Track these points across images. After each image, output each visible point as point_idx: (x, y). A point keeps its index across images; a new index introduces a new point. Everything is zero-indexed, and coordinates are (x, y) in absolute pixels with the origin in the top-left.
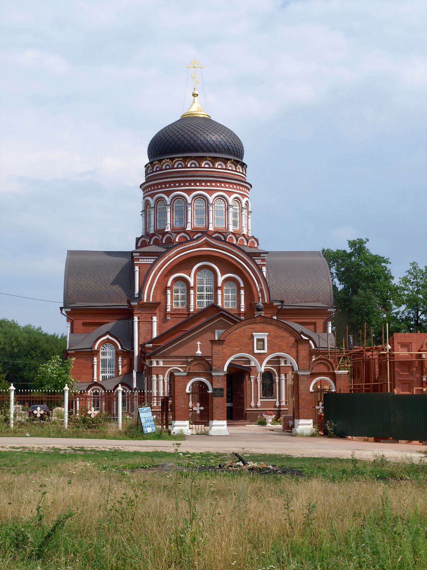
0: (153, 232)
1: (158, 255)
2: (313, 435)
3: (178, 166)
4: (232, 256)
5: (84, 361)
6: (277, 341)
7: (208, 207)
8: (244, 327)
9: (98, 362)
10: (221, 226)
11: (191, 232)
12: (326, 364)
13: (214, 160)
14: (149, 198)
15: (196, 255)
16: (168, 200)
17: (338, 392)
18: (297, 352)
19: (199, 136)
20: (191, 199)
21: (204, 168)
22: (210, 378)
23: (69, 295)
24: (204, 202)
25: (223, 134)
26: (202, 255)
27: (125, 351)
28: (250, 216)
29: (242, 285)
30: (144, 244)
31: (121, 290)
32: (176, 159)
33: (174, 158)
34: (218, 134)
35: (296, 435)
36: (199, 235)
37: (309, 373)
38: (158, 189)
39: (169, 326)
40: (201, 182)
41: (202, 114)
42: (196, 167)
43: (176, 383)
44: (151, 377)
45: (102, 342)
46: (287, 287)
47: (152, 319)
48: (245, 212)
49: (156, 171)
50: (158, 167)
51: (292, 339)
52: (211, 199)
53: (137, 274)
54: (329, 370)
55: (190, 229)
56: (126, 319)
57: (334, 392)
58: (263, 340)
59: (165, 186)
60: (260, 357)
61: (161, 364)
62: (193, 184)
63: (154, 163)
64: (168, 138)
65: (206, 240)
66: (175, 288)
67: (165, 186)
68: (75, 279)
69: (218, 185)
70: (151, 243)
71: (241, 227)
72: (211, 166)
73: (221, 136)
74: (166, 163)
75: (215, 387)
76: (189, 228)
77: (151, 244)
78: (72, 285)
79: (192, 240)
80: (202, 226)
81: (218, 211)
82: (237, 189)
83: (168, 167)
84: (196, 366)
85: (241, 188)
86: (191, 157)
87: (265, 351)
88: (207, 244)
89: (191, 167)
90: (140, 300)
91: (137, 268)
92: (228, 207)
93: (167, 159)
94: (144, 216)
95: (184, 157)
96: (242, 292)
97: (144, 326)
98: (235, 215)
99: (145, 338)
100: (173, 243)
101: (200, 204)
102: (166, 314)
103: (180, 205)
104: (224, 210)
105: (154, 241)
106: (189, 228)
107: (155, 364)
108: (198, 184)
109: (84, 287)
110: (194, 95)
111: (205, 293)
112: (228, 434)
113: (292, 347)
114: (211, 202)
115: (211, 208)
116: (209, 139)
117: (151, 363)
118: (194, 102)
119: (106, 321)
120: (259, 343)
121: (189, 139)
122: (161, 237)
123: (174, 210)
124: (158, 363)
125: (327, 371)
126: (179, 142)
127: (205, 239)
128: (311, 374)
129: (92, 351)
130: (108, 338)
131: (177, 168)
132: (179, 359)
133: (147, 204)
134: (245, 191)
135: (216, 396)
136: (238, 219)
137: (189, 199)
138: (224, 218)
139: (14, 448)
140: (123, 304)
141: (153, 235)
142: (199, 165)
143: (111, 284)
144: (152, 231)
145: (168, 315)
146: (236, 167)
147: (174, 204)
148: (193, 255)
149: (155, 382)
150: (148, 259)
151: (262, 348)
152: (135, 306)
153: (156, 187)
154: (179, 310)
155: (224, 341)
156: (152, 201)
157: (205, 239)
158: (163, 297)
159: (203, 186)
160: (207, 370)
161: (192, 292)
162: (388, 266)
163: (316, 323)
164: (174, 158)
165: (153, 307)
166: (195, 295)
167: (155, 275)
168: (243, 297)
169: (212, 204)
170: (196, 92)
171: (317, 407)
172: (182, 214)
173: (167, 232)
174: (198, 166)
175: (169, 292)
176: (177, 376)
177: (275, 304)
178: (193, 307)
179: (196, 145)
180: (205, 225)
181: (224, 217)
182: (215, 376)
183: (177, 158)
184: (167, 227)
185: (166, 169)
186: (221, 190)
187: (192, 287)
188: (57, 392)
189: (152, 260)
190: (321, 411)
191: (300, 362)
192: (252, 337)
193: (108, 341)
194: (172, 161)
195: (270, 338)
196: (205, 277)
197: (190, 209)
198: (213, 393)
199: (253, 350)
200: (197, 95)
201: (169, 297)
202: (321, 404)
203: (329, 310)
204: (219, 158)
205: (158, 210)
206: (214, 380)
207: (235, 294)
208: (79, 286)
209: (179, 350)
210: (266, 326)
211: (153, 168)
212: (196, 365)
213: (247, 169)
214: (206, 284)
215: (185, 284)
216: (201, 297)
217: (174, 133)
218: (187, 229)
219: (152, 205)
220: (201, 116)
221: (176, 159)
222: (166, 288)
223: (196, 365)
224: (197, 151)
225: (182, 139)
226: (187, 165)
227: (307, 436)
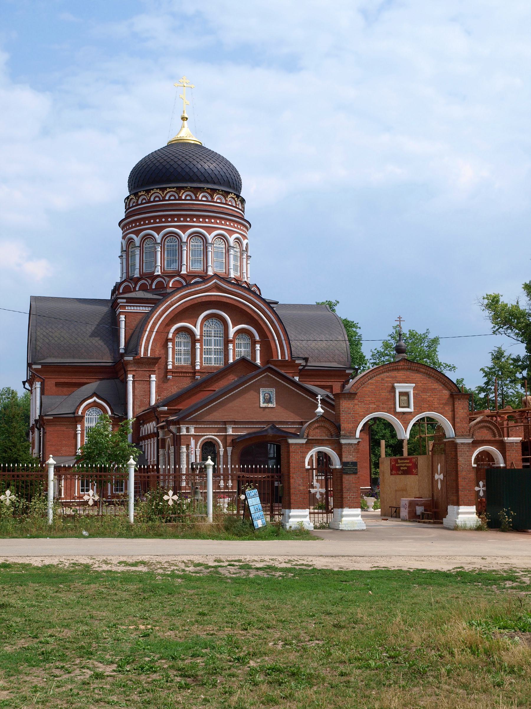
0: (138, 276)
1: (156, 303)
2: (479, 529)
3: (169, 196)
4: (239, 304)
5: (64, 428)
6: (425, 396)
7: (206, 247)
8: (382, 375)
9: (82, 430)
11: (188, 276)
12: (490, 428)
13: (196, 190)
16: (158, 237)
17: (508, 468)
18: (453, 411)
19: (195, 163)
20: (186, 237)
21: (201, 201)
22: (339, 448)
23: (38, 348)
26: (210, 301)
27: (116, 416)
29: (257, 338)
30: (127, 290)
31: (102, 344)
35: (456, 528)
36: (197, 279)
37: (470, 441)
38: (145, 224)
39: (174, 388)
40: (204, 217)
42: (160, 201)
43: (291, 454)
44: (180, 449)
45: (87, 405)
47: (150, 377)
49: (142, 204)
50: (144, 199)
51: (446, 393)
52: (210, 238)
54: (495, 436)
55: (186, 273)
57: (503, 467)
58: (407, 394)
60: (404, 417)
61: (192, 432)
62: (176, 219)
68: (44, 329)
69: (218, 221)
70: (137, 289)
72: (210, 199)
74: (155, 194)
75: (345, 460)
76: (184, 272)
77: (137, 289)
78: (42, 336)
79: (189, 285)
81: (208, 253)
82: (238, 228)
83: (157, 199)
84: (316, 430)
85: (242, 228)
87: (411, 409)
90: (136, 354)
91: (122, 317)
92: (228, 248)
93: (157, 189)
95: (177, 188)
96: (258, 347)
97: (140, 386)
98: (235, 256)
99: (141, 401)
100: (166, 288)
101: (198, 243)
102: (167, 371)
103: (173, 244)
104: (224, 252)
105: (140, 286)
106: (184, 272)
107: (184, 432)
109: (56, 339)
110: (184, 119)
111: (213, 347)
112: (365, 528)
113: (446, 404)
114: (210, 241)
115: (210, 249)
116: (206, 167)
117: (179, 430)
119: (85, 381)
120: (403, 398)
121: (183, 166)
122: (150, 281)
124: (188, 429)
125: (493, 439)
126: (172, 170)
127: (214, 281)
128: (473, 442)
129: (75, 417)
130: (95, 401)
131: (169, 200)
132: (215, 425)
133: (130, 242)
135: (347, 473)
137: (184, 237)
138: (224, 261)
139: (126, 564)
140: (107, 360)
141: (139, 279)
142: (196, 197)
145: (169, 374)
147: (166, 243)
148: (200, 300)
149: (185, 454)
150: (137, 306)
151: (406, 405)
153: (134, 225)
154: (182, 367)
155: (356, 394)
156: (137, 240)
157: (214, 281)
158: (163, 352)
159: (200, 222)
160: (332, 435)
161: (198, 345)
162: (358, 330)
163: (332, 386)
164: (165, 189)
165: (153, 363)
166: (201, 349)
167: (155, 324)
169: (211, 244)
170: (186, 116)
171: (477, 489)
172: (176, 254)
173: (158, 276)
174: (194, 198)
175: (170, 345)
176: (292, 444)
177: (297, 362)
178: (199, 363)
182: (345, 444)
183: (170, 188)
185: (154, 201)
187: (198, 340)
188: (18, 469)
190: (481, 494)
191: (458, 425)
192: (393, 389)
193: (95, 404)
194: (163, 192)
195: (416, 392)
196: (214, 328)
197: (185, 248)
198: (342, 469)
199: (395, 408)
201: (170, 351)
202: (481, 483)
203: (347, 371)
205: (144, 250)
206: (343, 449)
208: (50, 338)
209: (215, 413)
210: (412, 374)
211: (138, 200)
212: (317, 428)
216: (209, 352)
220: (193, 142)
221: (168, 190)
222: (167, 340)
223: (317, 428)
224: (193, 181)
225: (175, 166)
227: (471, 529)
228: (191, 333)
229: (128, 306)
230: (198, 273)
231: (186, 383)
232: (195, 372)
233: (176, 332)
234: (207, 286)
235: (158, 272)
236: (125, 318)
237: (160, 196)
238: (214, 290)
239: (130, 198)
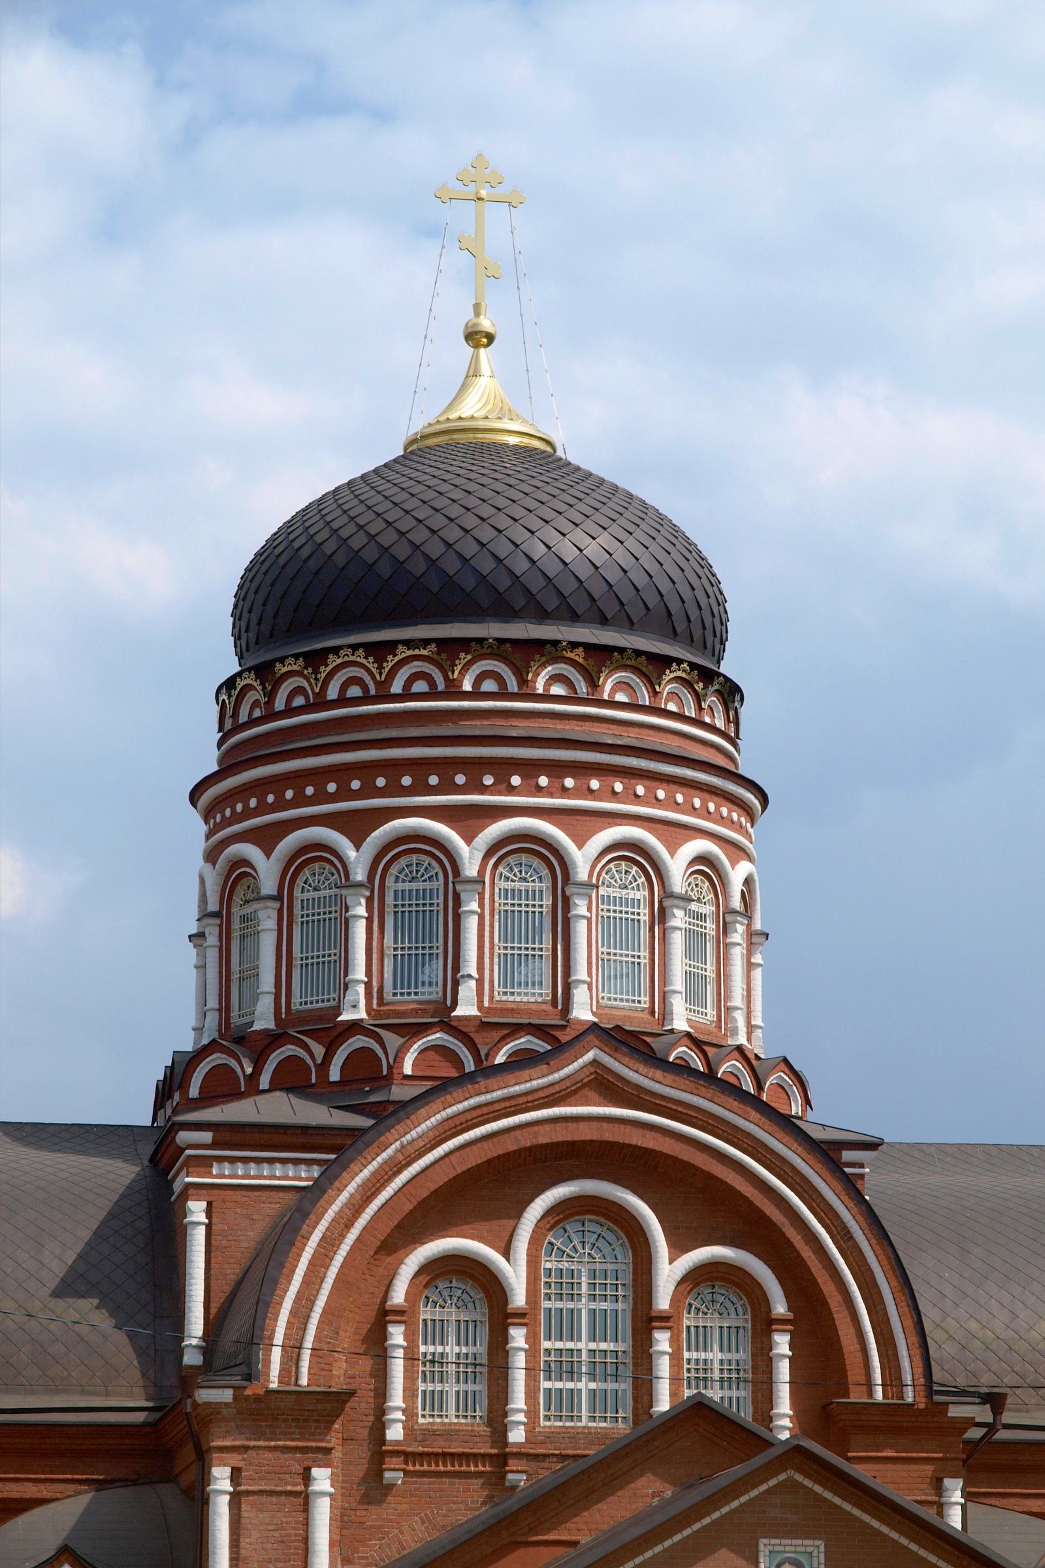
0: (271, 1025)
1: (339, 1147)
7: (567, 901)
10: (629, 1004)
14: (251, 851)
15: (543, 1140)
16: (357, 859)
19: (520, 535)
20: (479, 856)
21: (546, 697)
24: (545, 872)
25: (638, 534)
26: (572, 1144)
28: (757, 959)
29: (780, 1308)
30: (223, 1087)
32: (403, 652)
33: (390, 647)
34: (615, 529)
38: (301, 800)
40: (530, 768)
41: (512, 431)
42: (366, 699)
46: (973, 1326)
47: (307, 1478)
48: (738, 935)
49: (289, 712)
50: (299, 690)
53: (198, 1238)
55: (473, 1011)
56: (135, 1483)
59: (299, 792)
63: (280, 669)
64: (329, 548)
65: (595, 1062)
66: (425, 1313)
67: (299, 792)
70: (265, 1081)
71: (724, 1011)
72: (583, 689)
73: (630, 543)
76: (466, 1008)
79: (487, 1071)
80: (531, 996)
82: (708, 815)
83: (354, 691)
85: (724, 811)
86: (480, 641)
88: (605, 1086)
89: (476, 695)
90: (249, 1378)
91: (197, 1210)
94: (212, 940)
95: (441, 642)
96: (782, 1343)
98: (694, 939)
102: (379, 1451)
103: (420, 885)
104: (645, 918)
105: (276, 1070)
106: (466, 1008)
108: (488, 780)
110: (477, 338)
111: (584, 1345)
115: (580, 907)
116: (570, 554)
118: (473, 372)
122: (319, 1051)
123: (389, 910)
127: (590, 1056)
131: (406, 696)
133: (238, 876)
134: (740, 829)
136: (710, 970)
138: (645, 961)
140: (125, 1399)
141: (273, 1040)
142: (523, 682)
143: (57, 1294)
144: (264, 1021)
146: (699, 699)
147: (390, 882)
148: (526, 1140)
150: (259, 1161)
152: (215, 1409)
154: (449, 1433)
156: (267, 869)
157: (590, 1056)
158: (365, 1364)
159: (539, 790)
161: (518, 1337)
165: (309, 1416)
166: (532, 1352)
168: (783, 1371)
169: (589, 885)
170: (486, 324)
173: (355, 1027)
174: (513, 685)
175: (397, 1335)
178: (521, 1417)
179: (504, 583)
180: (547, 991)
181: (644, 953)
184: (349, 997)
186: (631, 814)
189: (316, 1172)
194: (380, 662)
196: (588, 1259)
197: (474, 906)
200: (490, 338)
204: (622, 650)
205: (297, 911)
207: (743, 1355)
211: (271, 695)
213: (744, 713)
214: (593, 1297)
215: (479, 1296)
216: (567, 1367)
217: (361, 521)
218: (457, 1013)
219: (268, 885)
220: (513, 440)
222: (384, 1315)
224: (508, 613)
226: (460, 681)
228: (490, 1285)
229: (221, 1159)
230: (531, 1013)
231: (463, 1505)
232: (502, 1458)
233: (424, 1279)
234: (556, 1076)
235: (356, 1011)
236: (209, 1213)
237: (367, 679)
238: (591, 1094)
239: (240, 684)
